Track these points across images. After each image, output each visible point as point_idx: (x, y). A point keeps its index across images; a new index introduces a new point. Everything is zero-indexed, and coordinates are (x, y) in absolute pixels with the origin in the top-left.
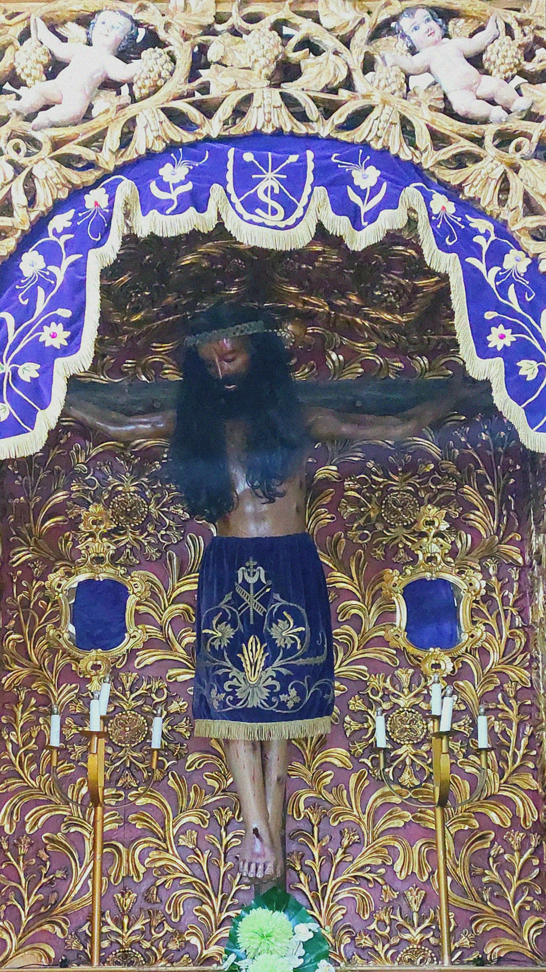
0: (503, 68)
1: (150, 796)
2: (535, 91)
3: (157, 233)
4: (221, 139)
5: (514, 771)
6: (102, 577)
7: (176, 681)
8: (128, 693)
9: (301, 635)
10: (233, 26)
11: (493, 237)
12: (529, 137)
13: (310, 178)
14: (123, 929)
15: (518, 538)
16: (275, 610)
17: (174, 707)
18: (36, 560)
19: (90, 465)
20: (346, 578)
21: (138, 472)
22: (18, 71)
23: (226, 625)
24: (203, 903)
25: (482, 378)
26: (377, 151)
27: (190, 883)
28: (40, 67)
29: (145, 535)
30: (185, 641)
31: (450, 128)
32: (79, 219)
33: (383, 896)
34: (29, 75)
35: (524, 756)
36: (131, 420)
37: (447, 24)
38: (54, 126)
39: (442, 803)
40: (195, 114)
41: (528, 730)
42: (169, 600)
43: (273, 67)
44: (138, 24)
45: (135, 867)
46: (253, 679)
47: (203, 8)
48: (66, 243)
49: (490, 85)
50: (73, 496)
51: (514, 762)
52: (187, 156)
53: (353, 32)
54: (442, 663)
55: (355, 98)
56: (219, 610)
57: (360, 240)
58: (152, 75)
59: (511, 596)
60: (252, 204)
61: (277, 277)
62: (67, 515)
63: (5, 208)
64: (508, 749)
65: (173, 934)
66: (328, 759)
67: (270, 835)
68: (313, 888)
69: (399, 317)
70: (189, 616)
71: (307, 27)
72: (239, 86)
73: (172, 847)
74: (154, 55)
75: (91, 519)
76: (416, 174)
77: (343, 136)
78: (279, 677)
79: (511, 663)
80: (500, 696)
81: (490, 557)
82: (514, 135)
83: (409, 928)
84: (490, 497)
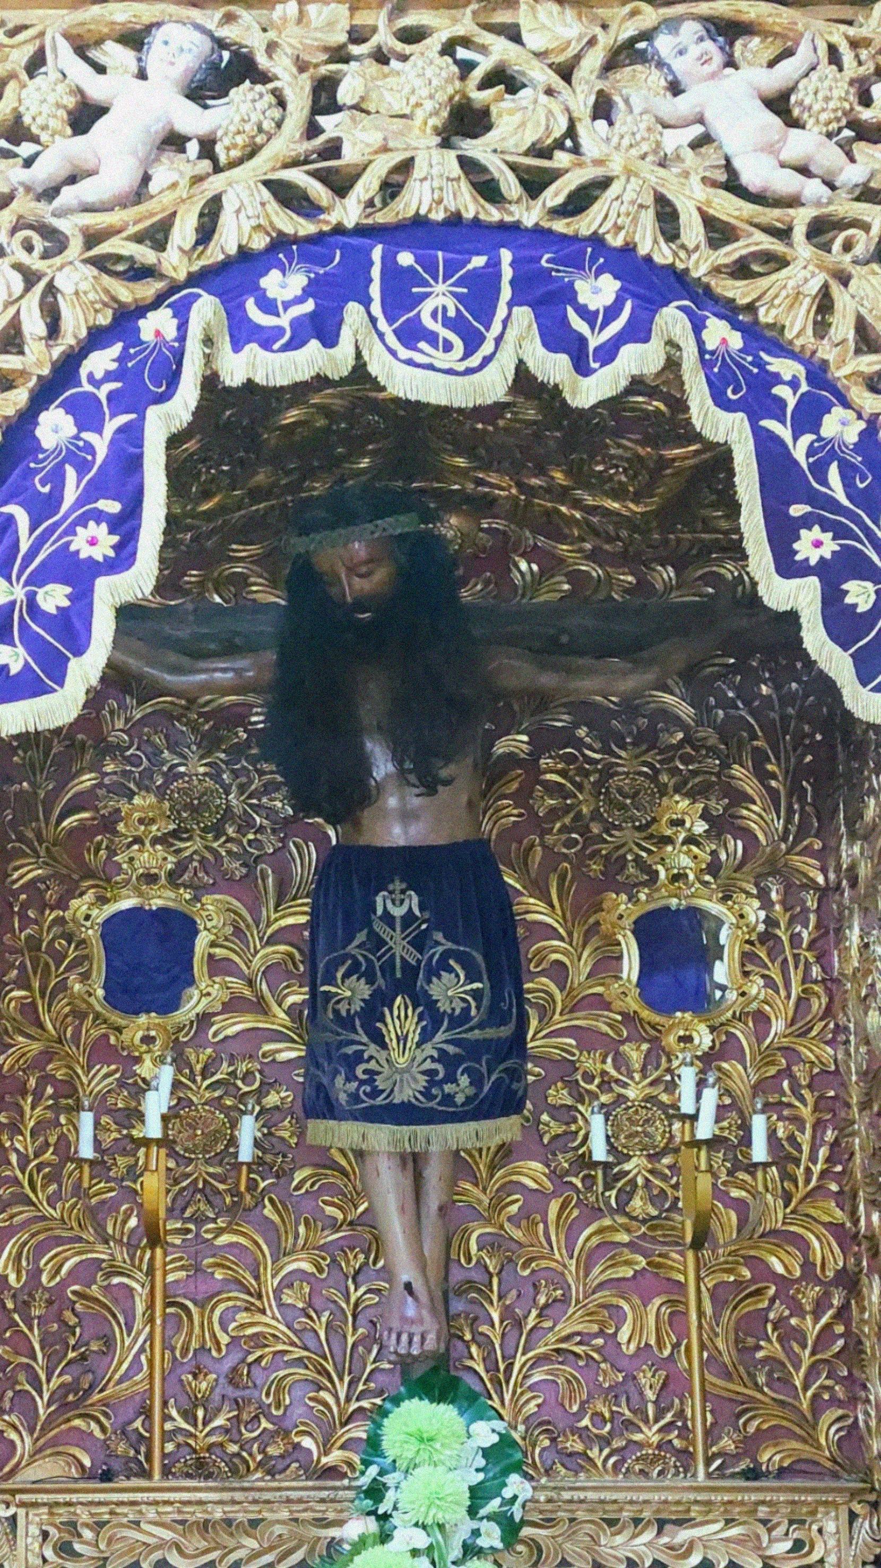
0: (824, 117)
1: (236, 1232)
2: (877, 154)
3: (257, 380)
4: (361, 231)
5: (808, 1195)
6: (156, 903)
7: (274, 1061)
8: (199, 1078)
9: (476, 994)
10: (379, 48)
11: (804, 388)
12: (866, 227)
13: (506, 293)
14: (195, 1425)
15: (818, 845)
17: (272, 1099)
18: (49, 877)
19: (132, 732)
20: (541, 906)
21: (209, 743)
22: (27, 120)
24: (320, 1388)
25: (783, 608)
26: (615, 249)
27: (300, 1359)
28: (62, 114)
29: (223, 839)
30: (291, 1000)
31: (737, 213)
32: (132, 357)
34: (44, 128)
35: (823, 1174)
36: (202, 664)
37: (731, 44)
38: (88, 209)
39: (697, 1245)
40: (319, 191)
41: (830, 1135)
42: (261, 939)
43: (445, 114)
44: (221, 44)
45: (214, 1336)
46: (401, 1060)
47: (330, 22)
48: (111, 396)
49: (803, 143)
52: (305, 258)
53: (578, 58)
54: (695, 1034)
55: (580, 165)
57: (589, 391)
58: (247, 127)
59: (805, 935)
60: (412, 334)
62: (97, 810)
63: (12, 340)
64: (797, 1162)
65: (273, 1435)
66: (514, 1178)
67: (430, 1292)
68: (492, 1367)
69: (632, 506)
70: (294, 964)
71: (500, 50)
72: (391, 144)
74: (250, 96)
75: (136, 815)
76: (677, 285)
77: (560, 226)
78: (443, 1056)
80: (786, 1084)
81: (771, 874)
82: (841, 225)
83: (641, 1425)
84: (773, 783)
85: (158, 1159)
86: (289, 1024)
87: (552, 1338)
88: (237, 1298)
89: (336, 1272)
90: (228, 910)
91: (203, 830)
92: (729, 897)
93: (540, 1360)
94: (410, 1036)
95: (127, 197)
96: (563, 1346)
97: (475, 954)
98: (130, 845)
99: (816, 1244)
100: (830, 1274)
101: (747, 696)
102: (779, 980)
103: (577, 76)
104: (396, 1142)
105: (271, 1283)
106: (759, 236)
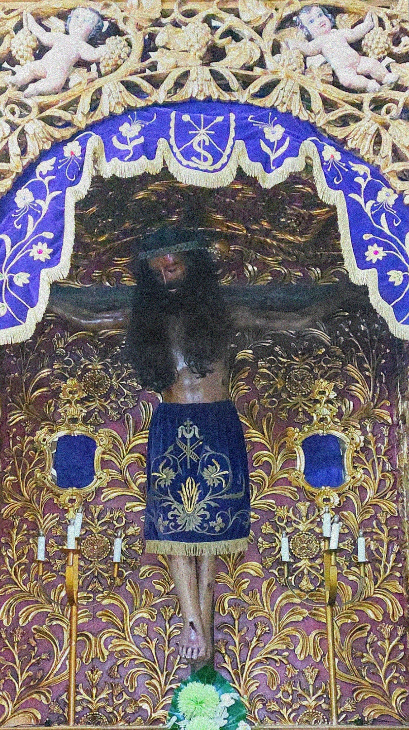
0: (376, 51)
1: (112, 598)
2: (401, 69)
4: (166, 105)
5: (385, 579)
6: (77, 433)
7: (132, 511)
8: (96, 520)
9: (226, 477)
11: (369, 178)
12: (397, 103)
13: (232, 134)
14: (92, 697)
15: (388, 404)
16: (206, 458)
17: (130, 531)
20: (259, 434)
21: (103, 355)
22: (14, 53)
24: (152, 678)
26: (283, 113)
27: (142, 663)
30: (139, 481)
31: (337, 96)
34: (22, 57)
35: (393, 567)
36: (99, 315)
37: (335, 18)
38: (40, 94)
39: (331, 603)
40: (146, 86)
41: (396, 548)
42: (126, 450)
43: (205, 50)
44: (103, 18)
45: (101, 651)
46: (189, 510)
48: (50, 183)
49: (368, 63)
50: (55, 372)
51: (385, 572)
52: (140, 117)
53: (265, 24)
54: (331, 498)
56: (164, 458)
57: (270, 180)
58: (114, 56)
59: (383, 448)
60: (189, 153)
61: (208, 208)
62: (50, 387)
63: (4, 156)
64: (380, 562)
66: (246, 570)
68: (235, 666)
69: (299, 238)
70: (142, 463)
71: (229, 21)
72: (179, 64)
74: (115, 42)
75: (68, 389)
77: (257, 102)
78: (209, 508)
80: (374, 523)
81: (367, 418)
83: (307, 696)
84: (367, 373)
85: (74, 559)
86: (139, 493)
88: (113, 632)
89: (160, 619)
95: (58, 88)
96: (269, 656)
98: (65, 404)
99: (389, 603)
100: (397, 619)
101: (354, 330)
102: (370, 470)
103: (265, 32)
104: (186, 551)
105: (129, 624)
106: (349, 107)
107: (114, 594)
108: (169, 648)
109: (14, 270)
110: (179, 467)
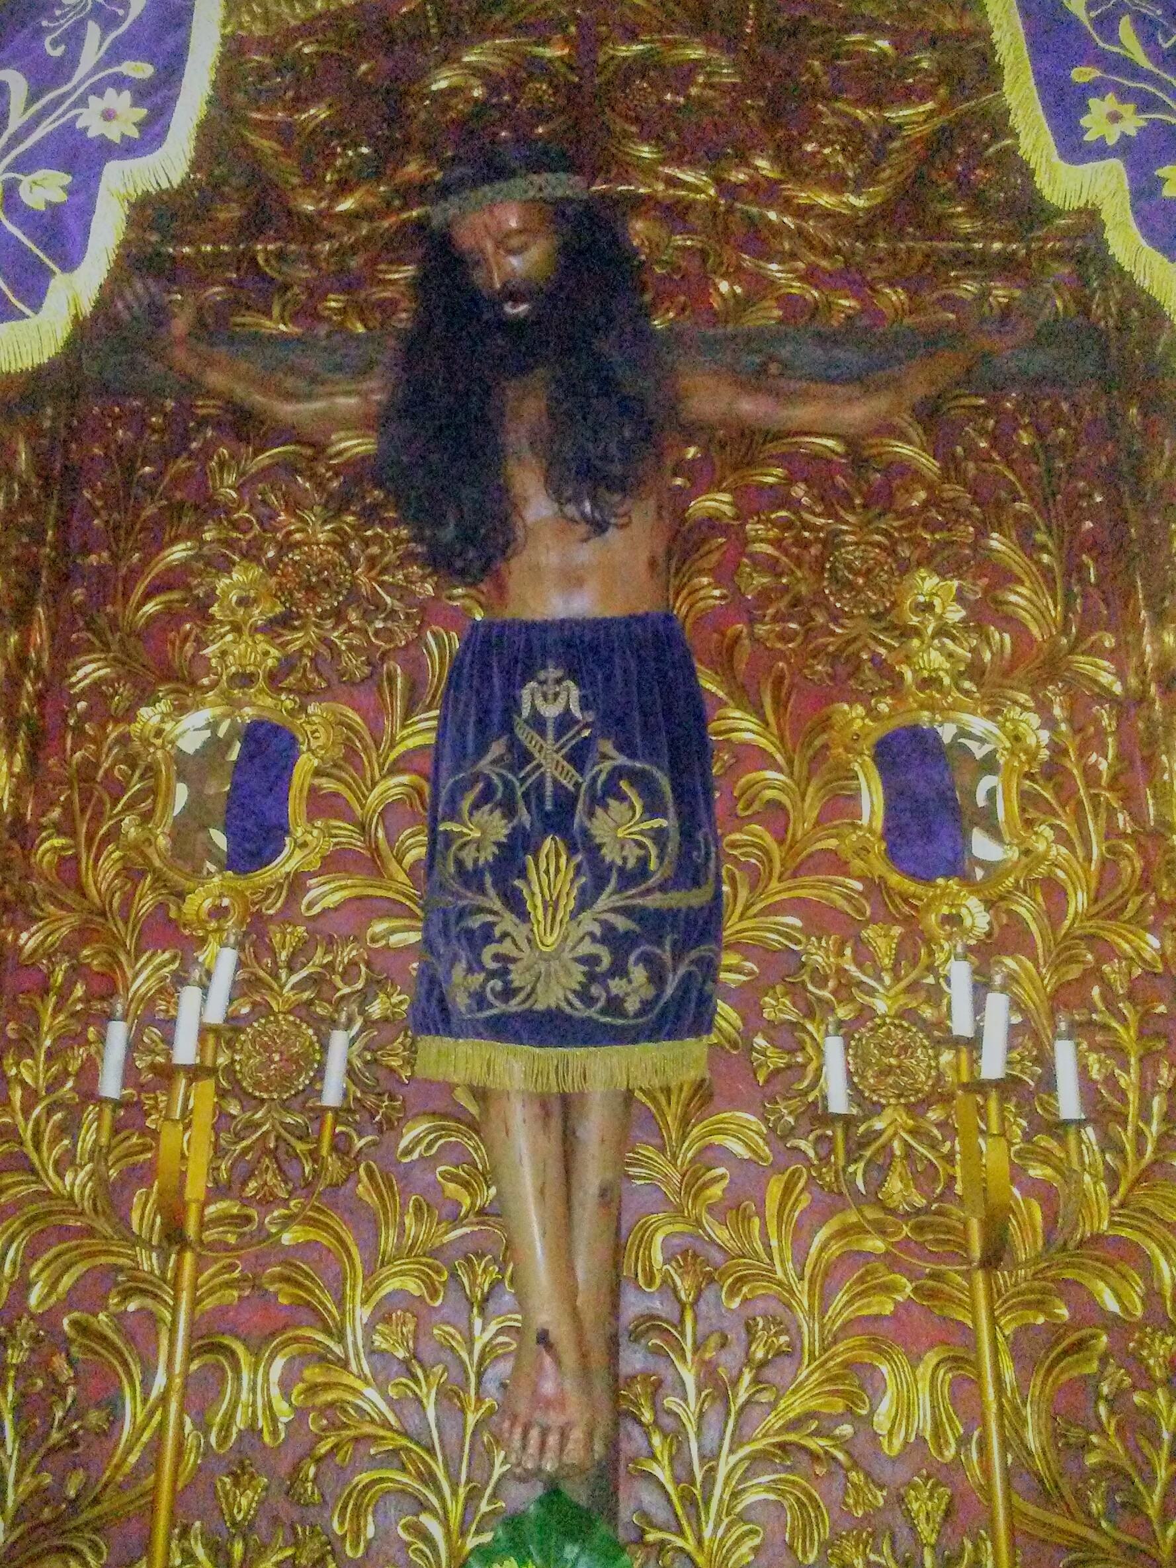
7: (387, 947)
8: (283, 974)
9: (659, 836)
15: (1109, 642)
16: (603, 777)
21: (337, 505)
23: (491, 811)
27: (395, 1452)
29: (342, 628)
30: (409, 858)
33: (851, 1501)
45: (269, 1405)
46: (550, 940)
50: (205, 550)
51: (1140, 1152)
54: (964, 911)
56: (477, 777)
59: (1103, 766)
61: (619, 125)
62: (189, 588)
66: (717, 1139)
67: (580, 1341)
68: (684, 1474)
69: (852, 199)
73: (357, 1355)
78: (609, 936)
79: (1113, 916)
80: (1096, 991)
84: (1045, 558)
87: (774, 1421)
90: (342, 724)
91: (321, 617)
92: (998, 712)
93: (759, 1460)
94: (563, 902)
96: (792, 1437)
97: (658, 774)
107: (318, 1210)
108: (479, 1400)
109: (25, 164)
110: (521, 805)
